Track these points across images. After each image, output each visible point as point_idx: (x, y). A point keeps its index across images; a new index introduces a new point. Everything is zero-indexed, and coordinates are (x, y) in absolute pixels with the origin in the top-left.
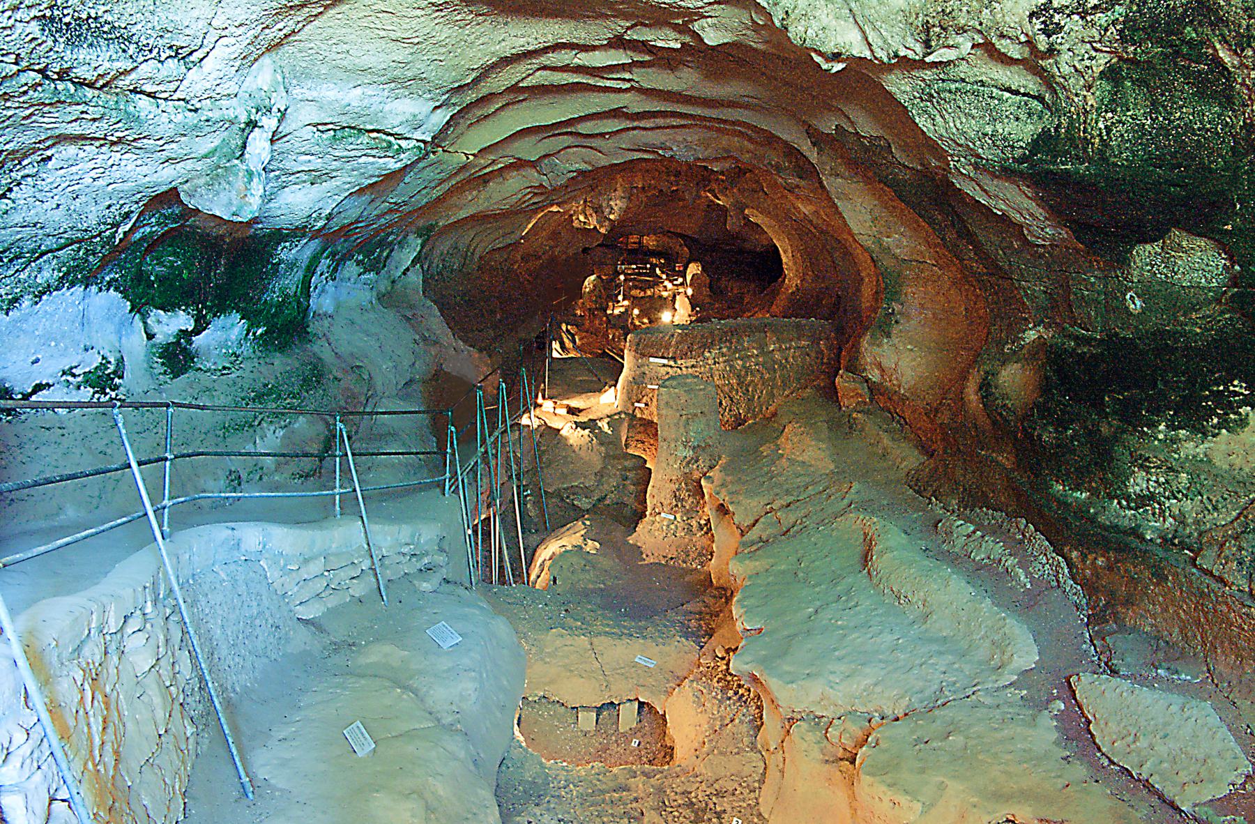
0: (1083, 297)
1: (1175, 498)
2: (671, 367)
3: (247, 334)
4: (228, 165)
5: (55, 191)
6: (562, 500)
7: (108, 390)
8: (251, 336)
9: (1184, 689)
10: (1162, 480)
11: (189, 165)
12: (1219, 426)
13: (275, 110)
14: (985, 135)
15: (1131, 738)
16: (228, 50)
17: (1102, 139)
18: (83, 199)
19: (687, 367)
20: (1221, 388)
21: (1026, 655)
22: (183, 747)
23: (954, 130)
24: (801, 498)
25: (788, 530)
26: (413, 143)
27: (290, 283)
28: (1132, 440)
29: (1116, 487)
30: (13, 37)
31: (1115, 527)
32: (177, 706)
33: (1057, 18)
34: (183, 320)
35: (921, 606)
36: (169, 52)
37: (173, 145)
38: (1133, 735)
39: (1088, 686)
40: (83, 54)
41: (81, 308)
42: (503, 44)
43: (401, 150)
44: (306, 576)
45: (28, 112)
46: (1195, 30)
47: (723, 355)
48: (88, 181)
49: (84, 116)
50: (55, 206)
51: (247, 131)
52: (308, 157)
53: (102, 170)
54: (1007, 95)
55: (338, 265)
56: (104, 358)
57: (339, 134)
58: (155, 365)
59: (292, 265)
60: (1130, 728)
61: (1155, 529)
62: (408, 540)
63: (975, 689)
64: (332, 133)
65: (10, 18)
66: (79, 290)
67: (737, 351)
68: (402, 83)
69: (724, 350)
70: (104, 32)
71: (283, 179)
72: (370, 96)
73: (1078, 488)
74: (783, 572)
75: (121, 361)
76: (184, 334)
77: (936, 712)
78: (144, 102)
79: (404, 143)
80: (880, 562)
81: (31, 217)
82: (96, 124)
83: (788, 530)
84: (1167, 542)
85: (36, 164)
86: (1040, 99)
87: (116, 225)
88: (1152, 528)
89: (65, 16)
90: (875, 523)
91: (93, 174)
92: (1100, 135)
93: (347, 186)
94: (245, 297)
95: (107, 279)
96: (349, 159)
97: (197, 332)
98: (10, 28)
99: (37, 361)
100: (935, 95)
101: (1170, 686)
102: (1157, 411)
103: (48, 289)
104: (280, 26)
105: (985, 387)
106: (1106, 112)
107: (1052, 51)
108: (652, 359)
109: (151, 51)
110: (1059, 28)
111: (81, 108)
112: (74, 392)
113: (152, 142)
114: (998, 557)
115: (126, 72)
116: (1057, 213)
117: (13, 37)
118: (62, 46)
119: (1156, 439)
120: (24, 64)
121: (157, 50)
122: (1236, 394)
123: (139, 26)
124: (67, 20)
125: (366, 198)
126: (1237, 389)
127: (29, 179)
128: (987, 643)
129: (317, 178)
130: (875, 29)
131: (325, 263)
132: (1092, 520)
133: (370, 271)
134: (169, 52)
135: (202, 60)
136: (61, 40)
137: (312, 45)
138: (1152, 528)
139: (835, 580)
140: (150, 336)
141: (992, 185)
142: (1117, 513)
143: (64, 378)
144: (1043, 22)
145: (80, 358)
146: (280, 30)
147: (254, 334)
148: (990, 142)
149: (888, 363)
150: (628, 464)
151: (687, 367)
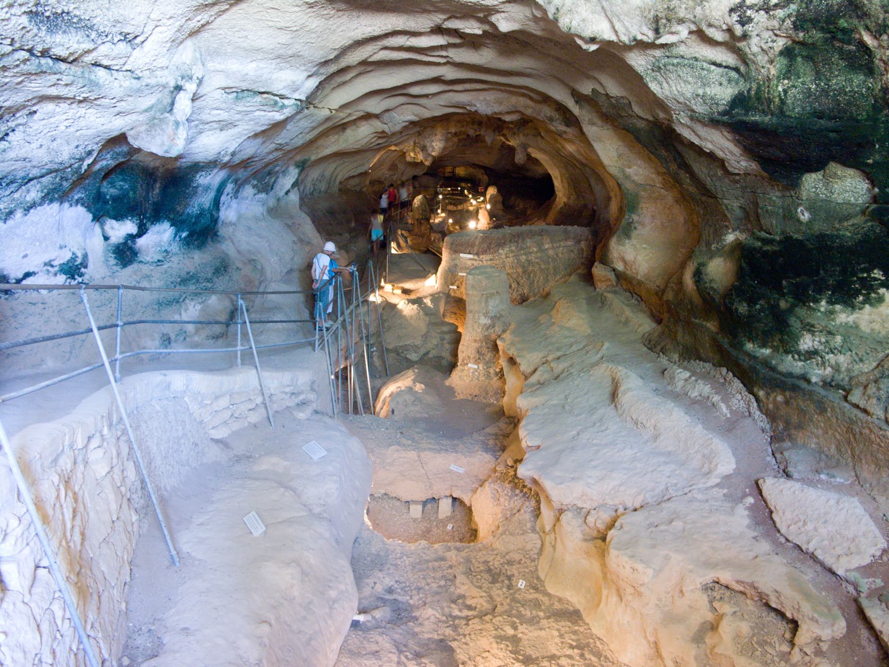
0: (767, 211)
1: (833, 353)
2: (475, 260)
3: (175, 237)
4: (161, 117)
5: (39, 136)
7: (76, 277)
8: (177, 238)
9: (839, 488)
10: (823, 340)
11: (134, 117)
12: (864, 302)
13: (195, 78)
14: (698, 95)
15: (801, 524)
16: (162, 36)
17: (781, 99)
18: (59, 141)
19: (486, 261)
20: (865, 275)
21: (726, 464)
22: (130, 529)
23: (676, 92)
25: (558, 376)
26: (292, 102)
27: (205, 200)
28: (801, 311)
29: (788, 346)
30: (9, 26)
31: (790, 375)
32: (125, 501)
33: (749, 13)
34: (129, 227)
35: (653, 430)
36: (119, 37)
37: (123, 103)
38: (802, 521)
39: (772, 486)
40: (59, 38)
41: (57, 218)
42: (357, 31)
43: (283, 107)
44: (217, 409)
45: (20, 79)
46: (846, 21)
47: (512, 252)
48: (62, 128)
49: (60, 82)
50: (39, 146)
51: (175, 93)
52: (219, 112)
53: (72, 121)
54: (713, 67)
55: (239, 188)
56: (73, 254)
57: (240, 95)
58: (110, 259)
59: (207, 188)
60: (801, 517)
61: (817, 375)
62: (289, 383)
63: (691, 488)
64: (235, 94)
65: (7, 12)
66: (55, 206)
67: (522, 249)
68: (285, 58)
69: (513, 248)
70: (74, 23)
71: (201, 126)
72: (262, 68)
73: (764, 345)
74: (555, 406)
75: (85, 256)
76: (132, 237)
77: (663, 505)
78: (101, 72)
79: (286, 102)
80: (625, 399)
81: (22, 153)
82: (68, 88)
83: (558, 376)
84: (827, 384)
85: (25, 117)
86: (737, 70)
87: (82, 160)
88: (817, 374)
89: (46, 11)
90: (621, 371)
91: (66, 123)
92: (780, 95)
93: (246, 132)
94: (173, 210)
95: (76, 197)
96: (247, 113)
97: (140, 234)
98: (7, 20)
99: (25, 256)
100: (663, 67)
101: (829, 487)
102: (820, 291)
103: (33, 205)
104: (199, 18)
105: (698, 274)
106: (784, 79)
107: (745, 36)
108: (462, 255)
109: (107, 36)
110: (750, 20)
111: (57, 76)
112: (53, 278)
113: (107, 100)
114: (707, 395)
115: (88, 52)
116: (749, 151)
117: (9, 26)
118: (44, 33)
119: (819, 311)
120: (17, 45)
121: (111, 35)
122: (875, 279)
123: (98, 19)
124: (47, 14)
125: (259, 140)
126: (876, 276)
127: (21, 127)
128: (699, 456)
129: (224, 126)
130: (619, 20)
131: (230, 187)
132: (773, 369)
133: (262, 192)
134: (119, 37)
135: (143, 42)
136: (44, 28)
137: (221, 32)
138: (817, 374)
139: (592, 410)
140: (106, 238)
141: (703, 131)
142: (790, 364)
143: (46, 268)
144: (739, 16)
145: (56, 254)
146: (199, 21)
147: (180, 237)
148: (701, 101)
149: (630, 257)
150: (445, 329)
151: (486, 261)
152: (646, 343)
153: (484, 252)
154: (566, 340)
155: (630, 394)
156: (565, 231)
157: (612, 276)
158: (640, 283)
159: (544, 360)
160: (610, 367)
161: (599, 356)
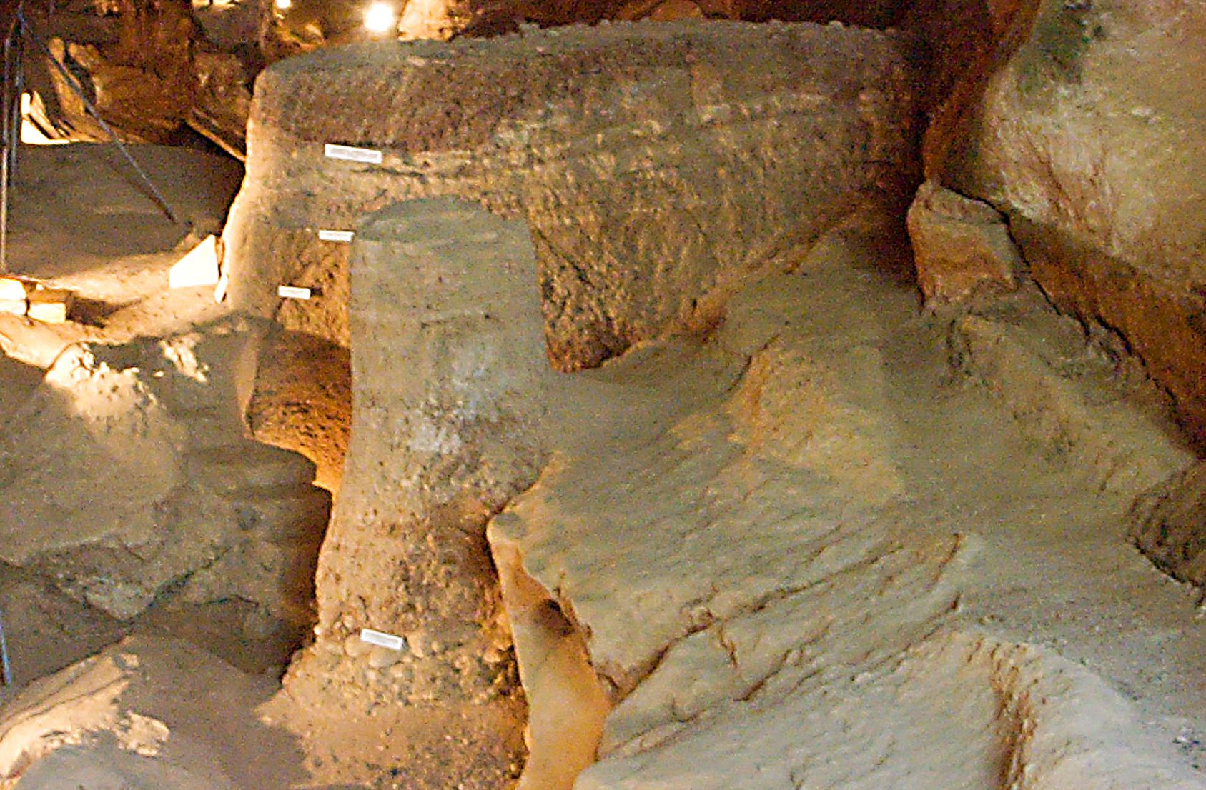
2: (393, 173)
6: (52, 588)
19: (441, 175)
24: (798, 583)
47: (556, 136)
151: (441, 175)
152: (1148, 539)
153: (433, 138)
154: (794, 526)
155: (1074, 763)
156: (790, 45)
157: (997, 245)
158: (1120, 275)
159: (697, 611)
160: (988, 643)
161: (940, 594)
